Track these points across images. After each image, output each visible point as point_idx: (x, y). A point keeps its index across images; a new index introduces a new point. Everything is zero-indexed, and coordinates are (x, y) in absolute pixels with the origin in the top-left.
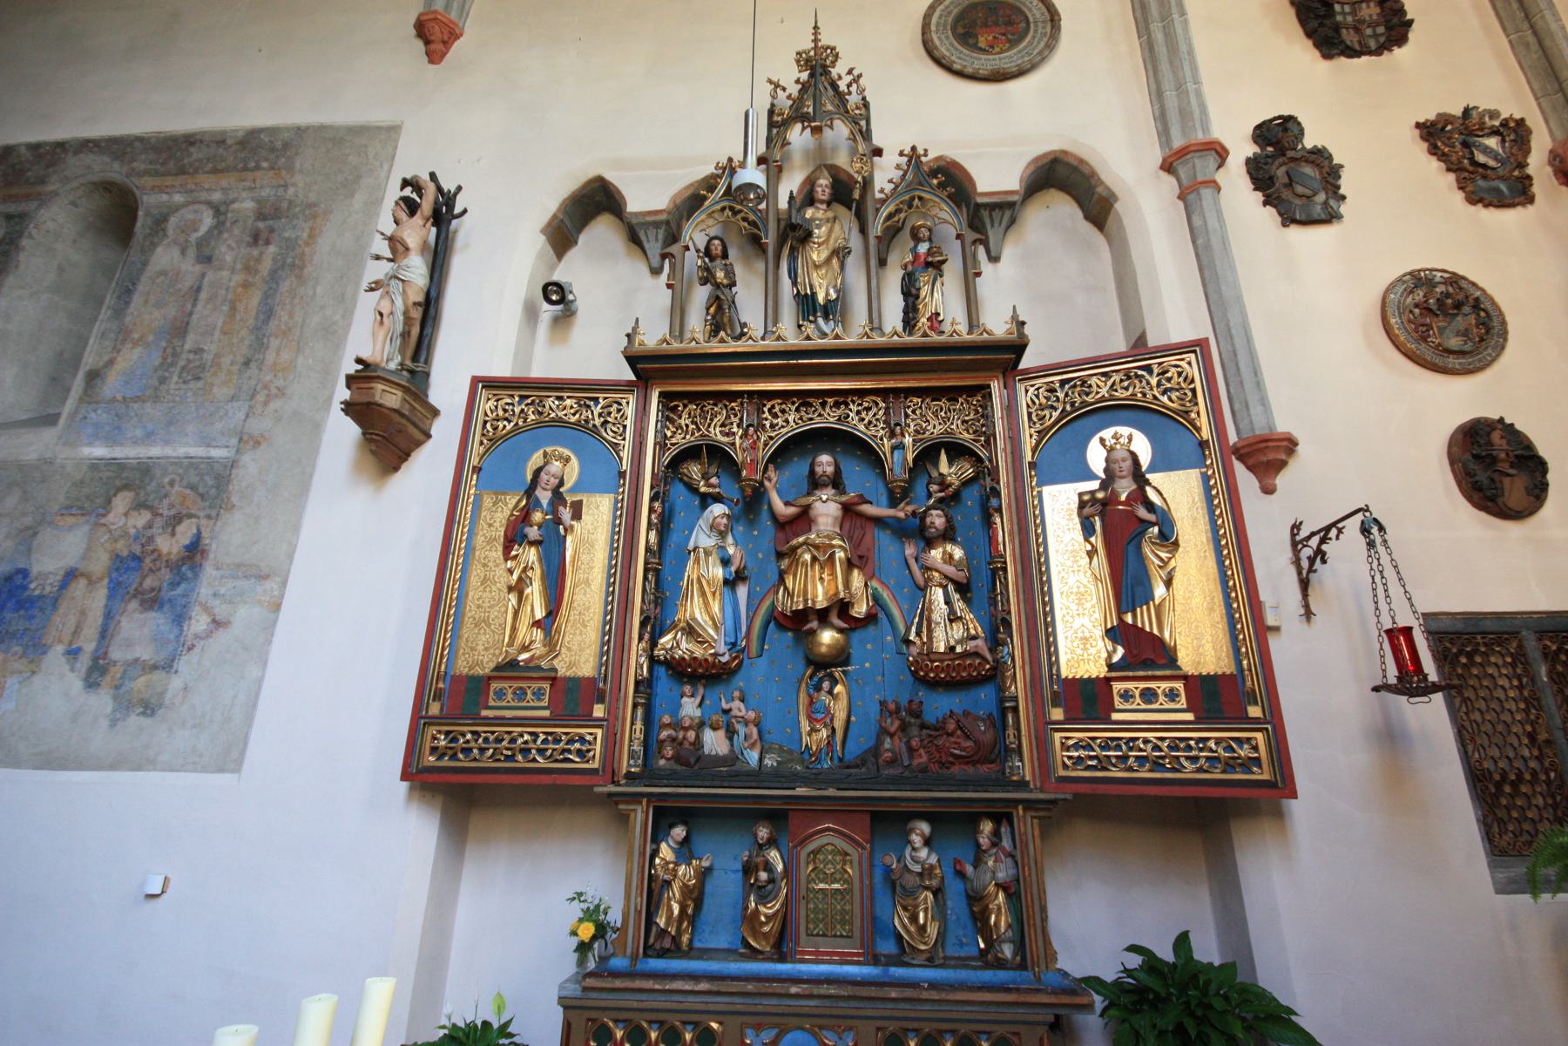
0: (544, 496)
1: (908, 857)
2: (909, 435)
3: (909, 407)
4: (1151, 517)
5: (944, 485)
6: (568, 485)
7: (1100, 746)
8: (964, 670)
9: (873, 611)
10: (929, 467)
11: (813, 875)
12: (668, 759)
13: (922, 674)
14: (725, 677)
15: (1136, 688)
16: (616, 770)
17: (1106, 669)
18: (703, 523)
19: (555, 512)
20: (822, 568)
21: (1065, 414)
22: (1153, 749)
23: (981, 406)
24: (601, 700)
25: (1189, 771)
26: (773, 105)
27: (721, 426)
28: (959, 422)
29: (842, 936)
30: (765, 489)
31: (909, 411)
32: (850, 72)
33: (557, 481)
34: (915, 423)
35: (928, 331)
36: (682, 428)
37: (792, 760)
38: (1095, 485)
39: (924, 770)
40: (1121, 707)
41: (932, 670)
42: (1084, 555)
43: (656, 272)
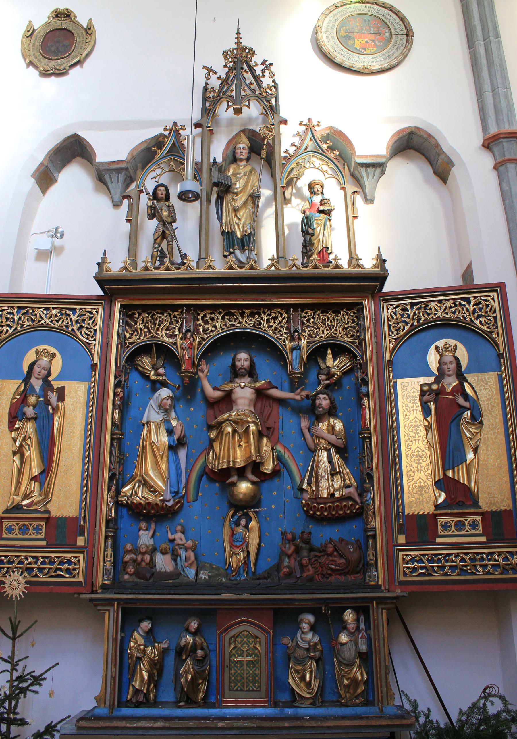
0: (37, 384)
1: (299, 639)
2: (305, 339)
3: (305, 317)
4: (467, 404)
5: (330, 375)
6: (55, 373)
7: (428, 560)
8: (341, 509)
9: (277, 468)
10: (320, 361)
11: (234, 652)
12: (131, 575)
13: (311, 512)
14: (170, 516)
15: (452, 521)
16: (94, 582)
17: (434, 508)
18: (153, 403)
19: (45, 396)
20: (240, 438)
21: (413, 327)
22: (460, 561)
23: (356, 317)
24: (82, 534)
25: (481, 574)
26: (207, 84)
27: (166, 330)
28: (341, 329)
29: (253, 690)
30: (199, 377)
31: (305, 320)
32: (263, 63)
33: (47, 371)
34: (308, 329)
35: (317, 264)
36: (137, 331)
37: (219, 575)
38: (431, 379)
39: (311, 579)
40: (443, 533)
41: (318, 510)
42: (423, 429)
43: (117, 205)
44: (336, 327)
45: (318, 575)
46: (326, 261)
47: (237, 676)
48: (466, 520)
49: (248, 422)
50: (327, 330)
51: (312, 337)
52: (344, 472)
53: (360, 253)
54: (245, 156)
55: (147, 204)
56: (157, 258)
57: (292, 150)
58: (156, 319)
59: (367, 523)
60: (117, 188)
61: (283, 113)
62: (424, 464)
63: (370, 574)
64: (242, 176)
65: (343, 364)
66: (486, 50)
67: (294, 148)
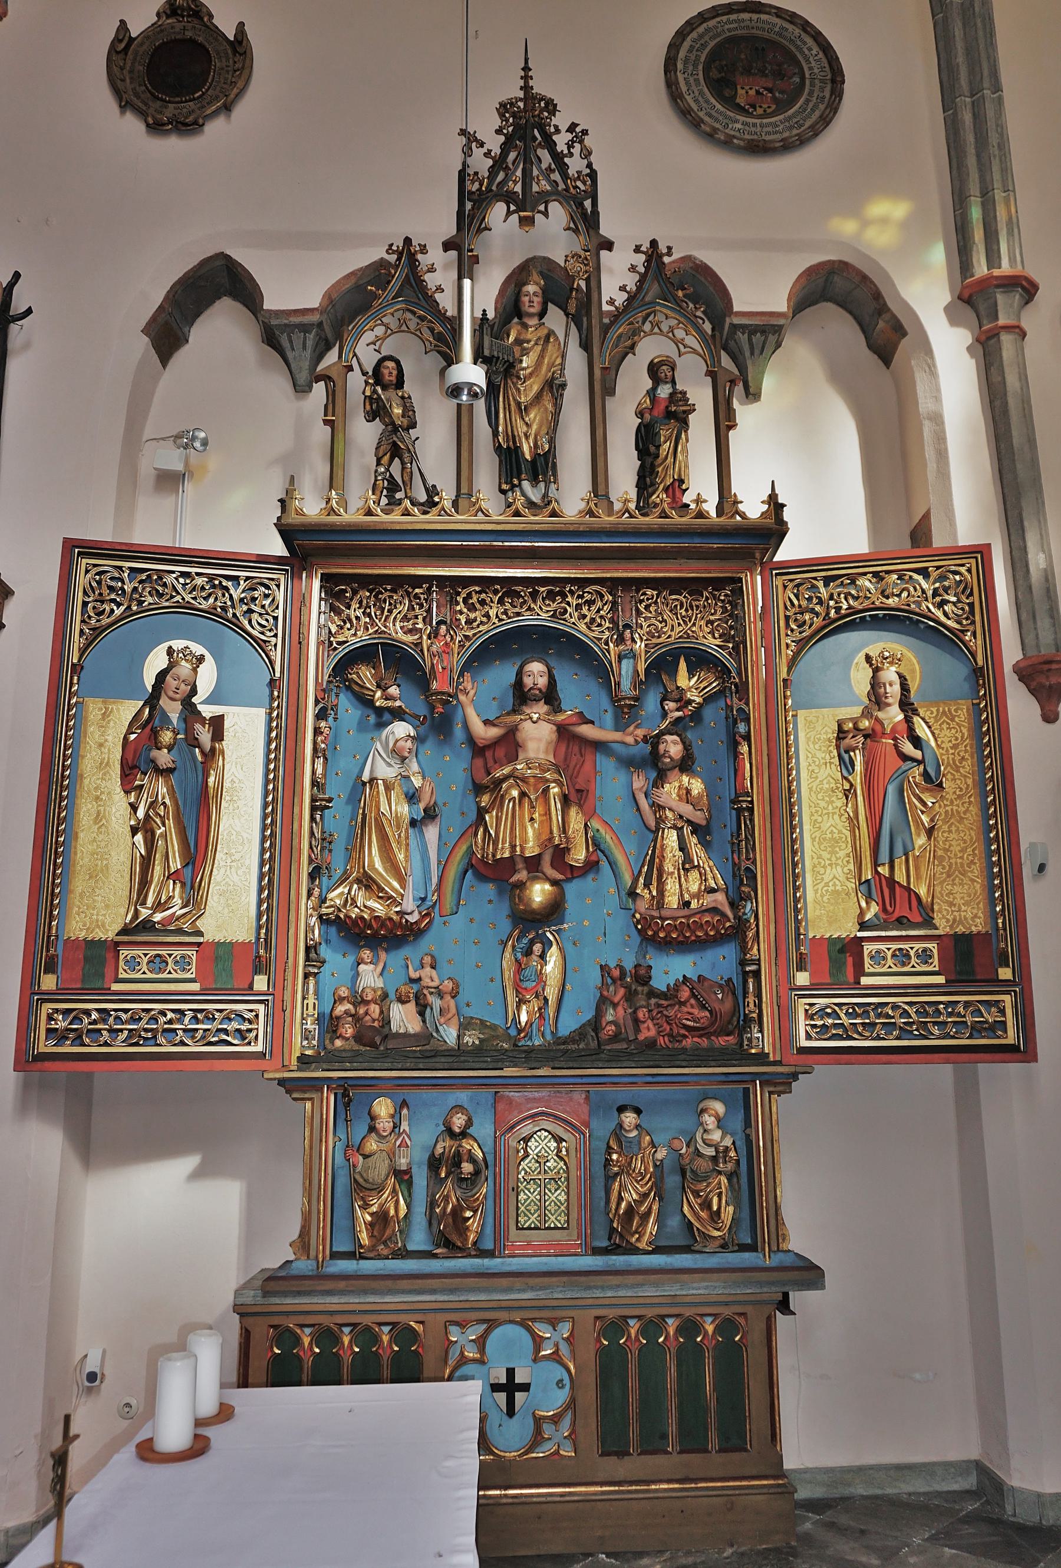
0: (173, 710)
3: (641, 601)
5: (683, 702)
7: (847, 1014)
9: (594, 858)
13: (650, 933)
15: (889, 949)
19: (189, 731)
23: (730, 602)
26: (465, 165)
28: (703, 623)
31: (642, 607)
32: (572, 128)
37: (497, 1037)
39: (651, 1044)
40: (872, 970)
42: (841, 795)
43: (301, 389)
44: (695, 620)
45: (663, 1036)
46: (679, 505)
47: (529, 1205)
48: (912, 948)
49: (547, 781)
50: (679, 624)
51: (653, 637)
52: (706, 866)
53: (738, 487)
54: (536, 309)
55: (364, 393)
56: (382, 492)
57: (621, 298)
58: (385, 601)
59: (744, 949)
60: (302, 359)
61: (606, 229)
62: (842, 854)
63: (749, 1035)
64: (533, 346)
65: (704, 684)
66: (975, 116)
67: (625, 296)
